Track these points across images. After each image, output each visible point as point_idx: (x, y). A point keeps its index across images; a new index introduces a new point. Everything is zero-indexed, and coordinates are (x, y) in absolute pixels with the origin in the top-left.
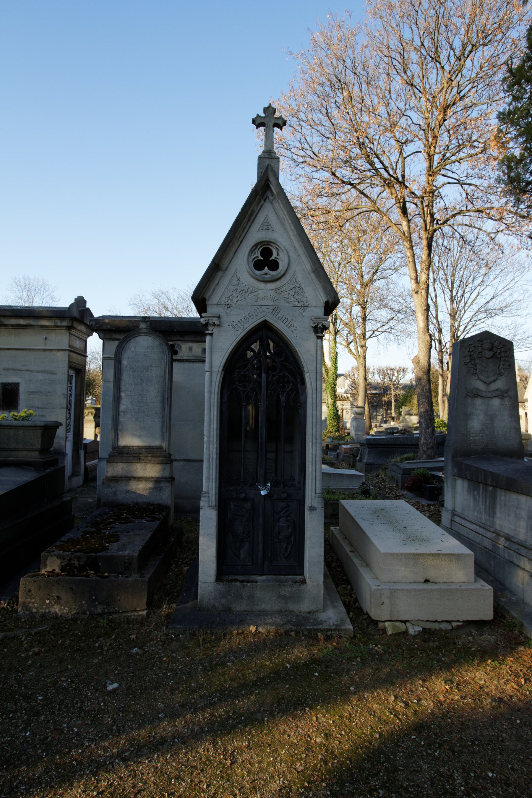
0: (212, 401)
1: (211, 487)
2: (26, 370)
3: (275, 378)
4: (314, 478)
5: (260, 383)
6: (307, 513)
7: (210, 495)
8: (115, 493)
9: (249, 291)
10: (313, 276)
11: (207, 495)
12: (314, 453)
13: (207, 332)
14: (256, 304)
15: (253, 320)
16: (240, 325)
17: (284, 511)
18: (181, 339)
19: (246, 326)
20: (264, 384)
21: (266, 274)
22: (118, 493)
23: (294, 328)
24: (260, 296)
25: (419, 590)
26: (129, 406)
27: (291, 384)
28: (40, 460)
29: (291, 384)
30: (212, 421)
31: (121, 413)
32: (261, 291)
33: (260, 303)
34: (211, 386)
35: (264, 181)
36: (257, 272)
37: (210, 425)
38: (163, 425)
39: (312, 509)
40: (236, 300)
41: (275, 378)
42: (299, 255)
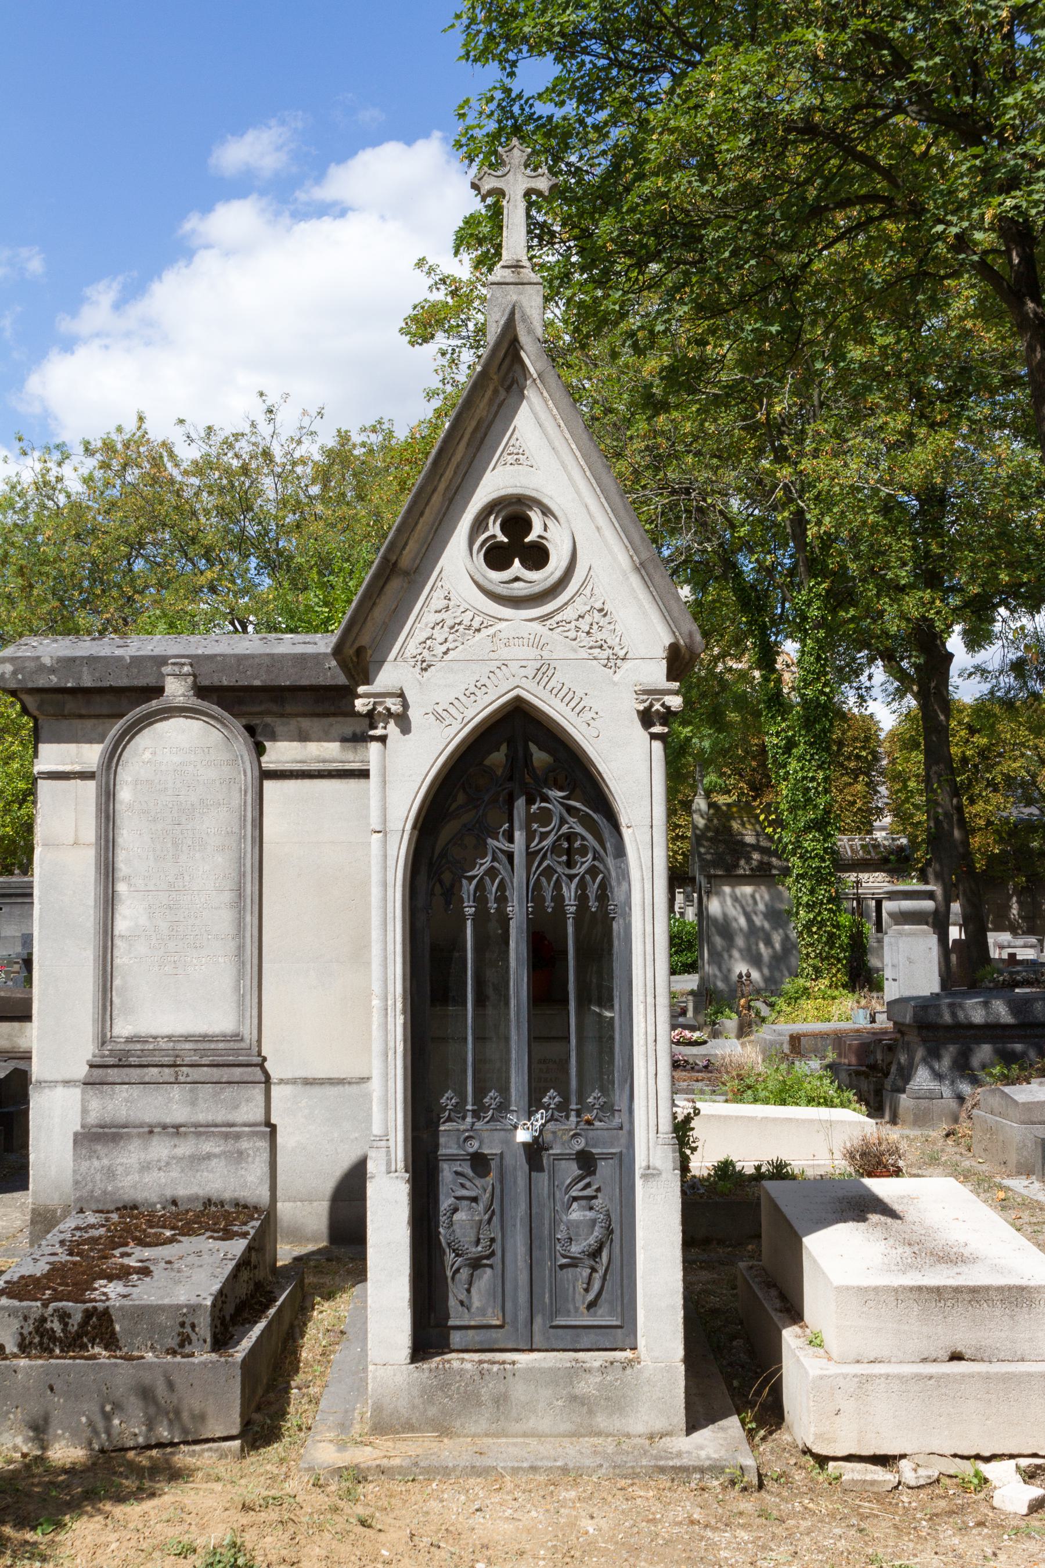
0: (390, 905)
1: (391, 1124)
3: (547, 842)
4: (652, 1095)
5: (510, 856)
6: (639, 1183)
7: (392, 1143)
8: (110, 1173)
9: (476, 624)
10: (635, 580)
12: (651, 1029)
13: (371, 733)
14: (492, 655)
18: (274, 708)
19: (469, 713)
20: (519, 860)
21: (517, 579)
22: (120, 1170)
23: (592, 714)
24: (501, 635)
25: (931, 1378)
26: (143, 921)
27: (590, 856)
29: (590, 856)
30: (390, 957)
31: (118, 942)
32: (504, 624)
33: (504, 653)
34: (385, 868)
35: (505, 345)
37: (386, 967)
38: (240, 975)
39: (651, 1174)
40: (444, 648)
41: (547, 842)
42: (598, 529)
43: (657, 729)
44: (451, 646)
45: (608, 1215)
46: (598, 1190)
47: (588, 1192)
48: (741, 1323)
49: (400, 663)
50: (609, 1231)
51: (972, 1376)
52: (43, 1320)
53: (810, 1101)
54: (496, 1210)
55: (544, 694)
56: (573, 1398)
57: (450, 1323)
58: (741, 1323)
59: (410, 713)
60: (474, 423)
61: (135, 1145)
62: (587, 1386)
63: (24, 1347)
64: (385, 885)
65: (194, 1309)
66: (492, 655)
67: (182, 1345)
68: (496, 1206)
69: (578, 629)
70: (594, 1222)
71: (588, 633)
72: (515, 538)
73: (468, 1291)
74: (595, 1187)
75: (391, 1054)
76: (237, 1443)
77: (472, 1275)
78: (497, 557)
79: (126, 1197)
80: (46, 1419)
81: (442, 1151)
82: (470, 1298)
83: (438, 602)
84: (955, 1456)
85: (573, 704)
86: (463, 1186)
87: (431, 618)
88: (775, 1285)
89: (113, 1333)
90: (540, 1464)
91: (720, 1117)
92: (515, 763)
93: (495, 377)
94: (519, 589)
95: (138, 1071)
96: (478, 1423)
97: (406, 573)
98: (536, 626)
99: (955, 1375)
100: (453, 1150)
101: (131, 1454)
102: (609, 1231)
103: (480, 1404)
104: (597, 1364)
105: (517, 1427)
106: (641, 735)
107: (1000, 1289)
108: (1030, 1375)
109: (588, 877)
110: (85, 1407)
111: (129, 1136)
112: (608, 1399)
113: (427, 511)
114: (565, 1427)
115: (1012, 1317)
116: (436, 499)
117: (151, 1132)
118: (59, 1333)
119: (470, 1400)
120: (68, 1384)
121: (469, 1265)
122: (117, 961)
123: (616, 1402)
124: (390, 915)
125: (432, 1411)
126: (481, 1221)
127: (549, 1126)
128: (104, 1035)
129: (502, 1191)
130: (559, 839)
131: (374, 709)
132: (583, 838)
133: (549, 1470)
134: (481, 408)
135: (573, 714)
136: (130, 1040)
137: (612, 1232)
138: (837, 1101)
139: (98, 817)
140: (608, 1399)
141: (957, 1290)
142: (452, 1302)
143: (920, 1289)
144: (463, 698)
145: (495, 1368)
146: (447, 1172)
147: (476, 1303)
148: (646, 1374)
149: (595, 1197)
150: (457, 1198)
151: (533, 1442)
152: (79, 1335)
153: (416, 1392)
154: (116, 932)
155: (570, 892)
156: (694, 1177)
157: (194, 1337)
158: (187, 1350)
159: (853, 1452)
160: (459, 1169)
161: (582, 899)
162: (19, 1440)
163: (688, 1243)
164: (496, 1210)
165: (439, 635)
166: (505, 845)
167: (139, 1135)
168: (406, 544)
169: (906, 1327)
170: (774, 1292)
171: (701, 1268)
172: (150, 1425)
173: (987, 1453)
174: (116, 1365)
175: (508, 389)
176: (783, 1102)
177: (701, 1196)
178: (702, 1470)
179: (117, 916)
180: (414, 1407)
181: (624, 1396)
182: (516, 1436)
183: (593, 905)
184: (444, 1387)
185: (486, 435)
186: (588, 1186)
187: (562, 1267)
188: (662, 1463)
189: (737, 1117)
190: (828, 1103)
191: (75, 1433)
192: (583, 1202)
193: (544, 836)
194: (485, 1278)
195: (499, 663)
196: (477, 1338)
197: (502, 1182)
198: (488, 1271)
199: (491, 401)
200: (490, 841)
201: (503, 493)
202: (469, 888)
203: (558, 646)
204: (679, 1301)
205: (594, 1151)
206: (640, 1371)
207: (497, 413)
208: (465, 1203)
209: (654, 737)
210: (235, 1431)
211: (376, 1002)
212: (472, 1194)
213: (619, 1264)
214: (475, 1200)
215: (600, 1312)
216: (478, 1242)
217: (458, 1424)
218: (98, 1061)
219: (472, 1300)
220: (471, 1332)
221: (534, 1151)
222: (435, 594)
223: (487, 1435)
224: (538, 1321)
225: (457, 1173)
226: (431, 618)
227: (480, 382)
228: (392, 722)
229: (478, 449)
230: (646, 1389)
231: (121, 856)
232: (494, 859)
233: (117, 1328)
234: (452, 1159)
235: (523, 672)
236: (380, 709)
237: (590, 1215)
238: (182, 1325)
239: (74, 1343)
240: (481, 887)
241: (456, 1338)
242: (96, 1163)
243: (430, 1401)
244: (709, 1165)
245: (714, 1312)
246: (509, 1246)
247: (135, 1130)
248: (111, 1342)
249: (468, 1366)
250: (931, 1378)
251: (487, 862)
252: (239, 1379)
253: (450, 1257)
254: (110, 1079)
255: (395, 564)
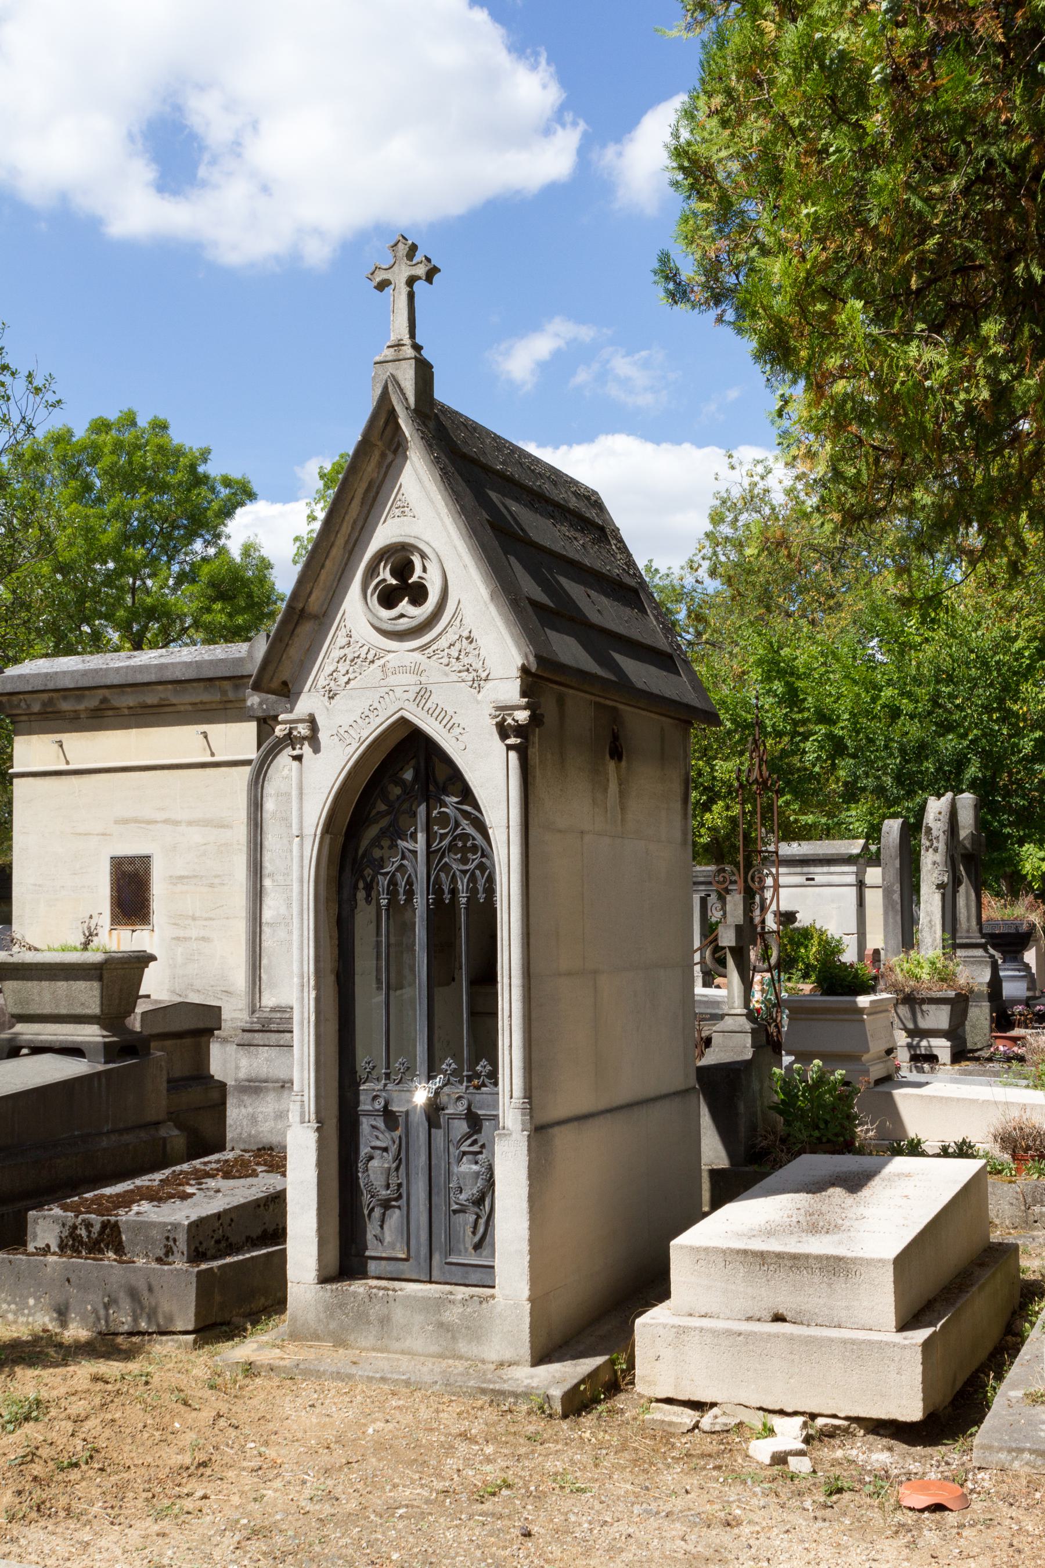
2: (166, 821)
7: (306, 1099)
8: (253, 1120)
9: (370, 657)
11: (299, 1098)
14: (382, 683)
15: (379, 720)
16: (351, 731)
17: (469, 1142)
22: (260, 1117)
23: (460, 730)
25: (740, 1334)
28: (100, 1039)
31: (264, 928)
32: (392, 655)
33: (392, 680)
36: (385, 614)
40: (346, 679)
42: (465, 566)
43: (512, 741)
44: (351, 676)
47: (475, 1148)
49: (313, 693)
51: (777, 1336)
52: (74, 1227)
54: (402, 1159)
55: (423, 714)
56: (441, 1325)
57: (367, 1253)
59: (320, 735)
60: (364, 486)
61: (271, 1097)
62: (452, 1315)
63: (62, 1247)
64: (301, 881)
65: (176, 1226)
66: (382, 683)
67: (167, 1255)
68: (403, 1155)
69: (449, 656)
70: (477, 1174)
71: (458, 659)
72: (401, 581)
73: (382, 1227)
75: (306, 1022)
76: (191, 1337)
77: (384, 1214)
78: (389, 598)
79: (265, 1140)
80: (67, 1308)
81: (362, 1107)
82: (383, 1233)
83: (342, 640)
84: (760, 1409)
85: (444, 722)
86: (377, 1137)
87: (336, 653)
89: (121, 1242)
90: (389, 1376)
91: (942, 1098)
92: (405, 771)
93: (379, 443)
94: (404, 624)
95: (277, 1035)
96: (366, 1339)
97: (316, 617)
98: (416, 654)
99: (762, 1334)
100: (369, 1108)
101: (120, 1339)
103: (369, 1323)
104: (459, 1297)
105: (397, 1345)
106: (499, 746)
107: (819, 1258)
108: (832, 1340)
109: (478, 872)
110: (91, 1297)
111: (267, 1089)
112: (468, 1328)
113: (328, 563)
114: (434, 1349)
115: (830, 1285)
116: (337, 552)
117: (283, 1087)
118: (85, 1239)
119: (361, 1318)
120: (80, 1278)
121: (381, 1205)
122: (264, 944)
123: (475, 1331)
124: (305, 906)
125: (333, 1325)
126: (389, 1169)
127: (446, 1089)
128: (254, 1005)
129: (407, 1143)
130: (454, 839)
131: (290, 733)
132: (474, 839)
133: (396, 1381)
134: (370, 469)
135: (445, 731)
136: (273, 1010)
139: (249, 824)
140: (468, 1328)
141: (779, 1256)
142: (369, 1236)
143: (745, 1252)
144: (359, 721)
145: (381, 1293)
146: (365, 1124)
147: (388, 1238)
148: (499, 1309)
149: (481, 1153)
150: (373, 1148)
151: (405, 1358)
152: (97, 1242)
153: (321, 1309)
154: (264, 920)
155: (462, 885)
157: (175, 1249)
158: (171, 1259)
159: (671, 1395)
160: (374, 1123)
161: (473, 891)
162: (47, 1319)
164: (402, 1159)
165: (343, 667)
166: (410, 845)
167: (274, 1089)
168: (311, 593)
169: (733, 1287)
172: (135, 1320)
173: (790, 1410)
174: (112, 1266)
175: (395, 452)
178: (516, 1395)
179: (264, 907)
180: (320, 1321)
181: (481, 1327)
182: (396, 1352)
183: (482, 897)
184: (341, 1305)
185: (377, 493)
186: (475, 1142)
187: (455, 1212)
188: (484, 1385)
189: (958, 1099)
191: (84, 1318)
192: (470, 1157)
193: (443, 837)
194: (395, 1217)
195: (387, 689)
196: (388, 1268)
197: (407, 1136)
198: (397, 1211)
199: (379, 464)
200: (399, 842)
201: (388, 542)
202: (383, 882)
203: (434, 671)
204: (525, 1247)
205: (480, 1112)
206: (493, 1306)
207: (386, 473)
208: (379, 1152)
209: (509, 748)
210: (190, 1328)
211: (296, 980)
212: (384, 1145)
214: (385, 1150)
215: (485, 1253)
216: (388, 1187)
217: (352, 1337)
218: (248, 1026)
219: (384, 1237)
220: (383, 1263)
221: (434, 1110)
222: (339, 633)
223: (374, 1349)
224: (436, 1258)
225: (373, 1127)
226: (336, 653)
227: (364, 447)
228: (306, 743)
229: (372, 506)
230: (498, 1322)
231: (267, 857)
232: (403, 857)
233: (124, 1238)
234: (368, 1114)
235: (406, 696)
236: (295, 733)
237: (475, 1168)
238: (168, 1238)
239: (95, 1247)
240: (393, 882)
241: (372, 1267)
242: (243, 1110)
243: (331, 1316)
246: (413, 1192)
247: (271, 1085)
248: (119, 1249)
249: (361, 1290)
250: (740, 1334)
251: (396, 860)
252: (194, 1285)
253: (366, 1198)
254: (256, 1042)
255: (303, 610)
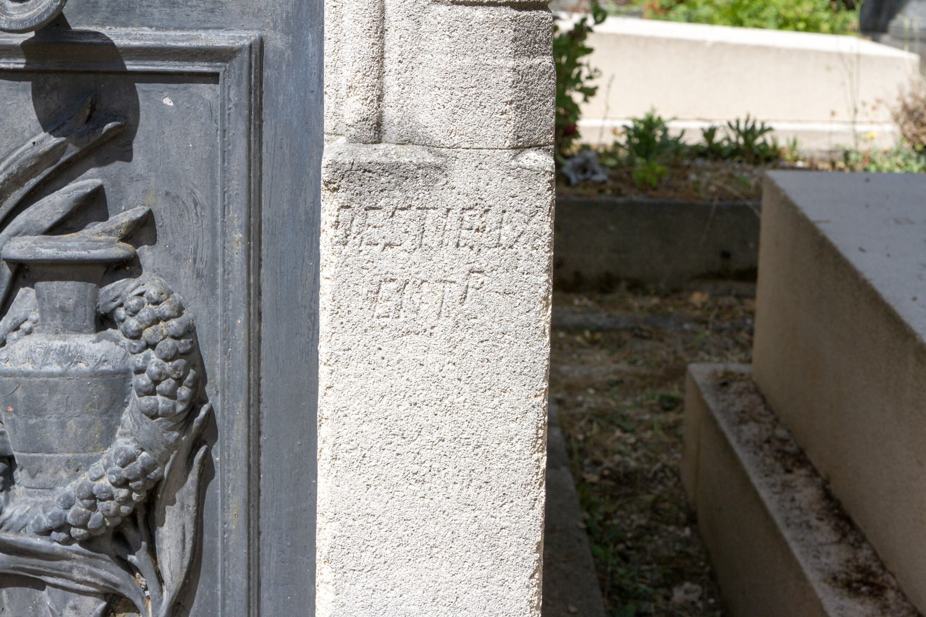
45: (189, 355)
46: (142, 230)
47: (94, 242)
48: (692, 520)
50: (195, 428)
53: (784, 24)
58: (692, 520)
70: (114, 386)
74: (122, 218)
88: (800, 459)
102: (195, 428)
137: (207, 433)
138: (825, 27)
149: (126, 267)
156: (586, 147)
163: (566, 282)
170: (807, 494)
171: (593, 343)
176: (739, 23)
177: (600, 187)
186: (92, 207)
190: (812, 27)
192: (66, 291)
213: (238, 578)
237: (95, 349)
244: (619, 124)
245: (624, 482)
